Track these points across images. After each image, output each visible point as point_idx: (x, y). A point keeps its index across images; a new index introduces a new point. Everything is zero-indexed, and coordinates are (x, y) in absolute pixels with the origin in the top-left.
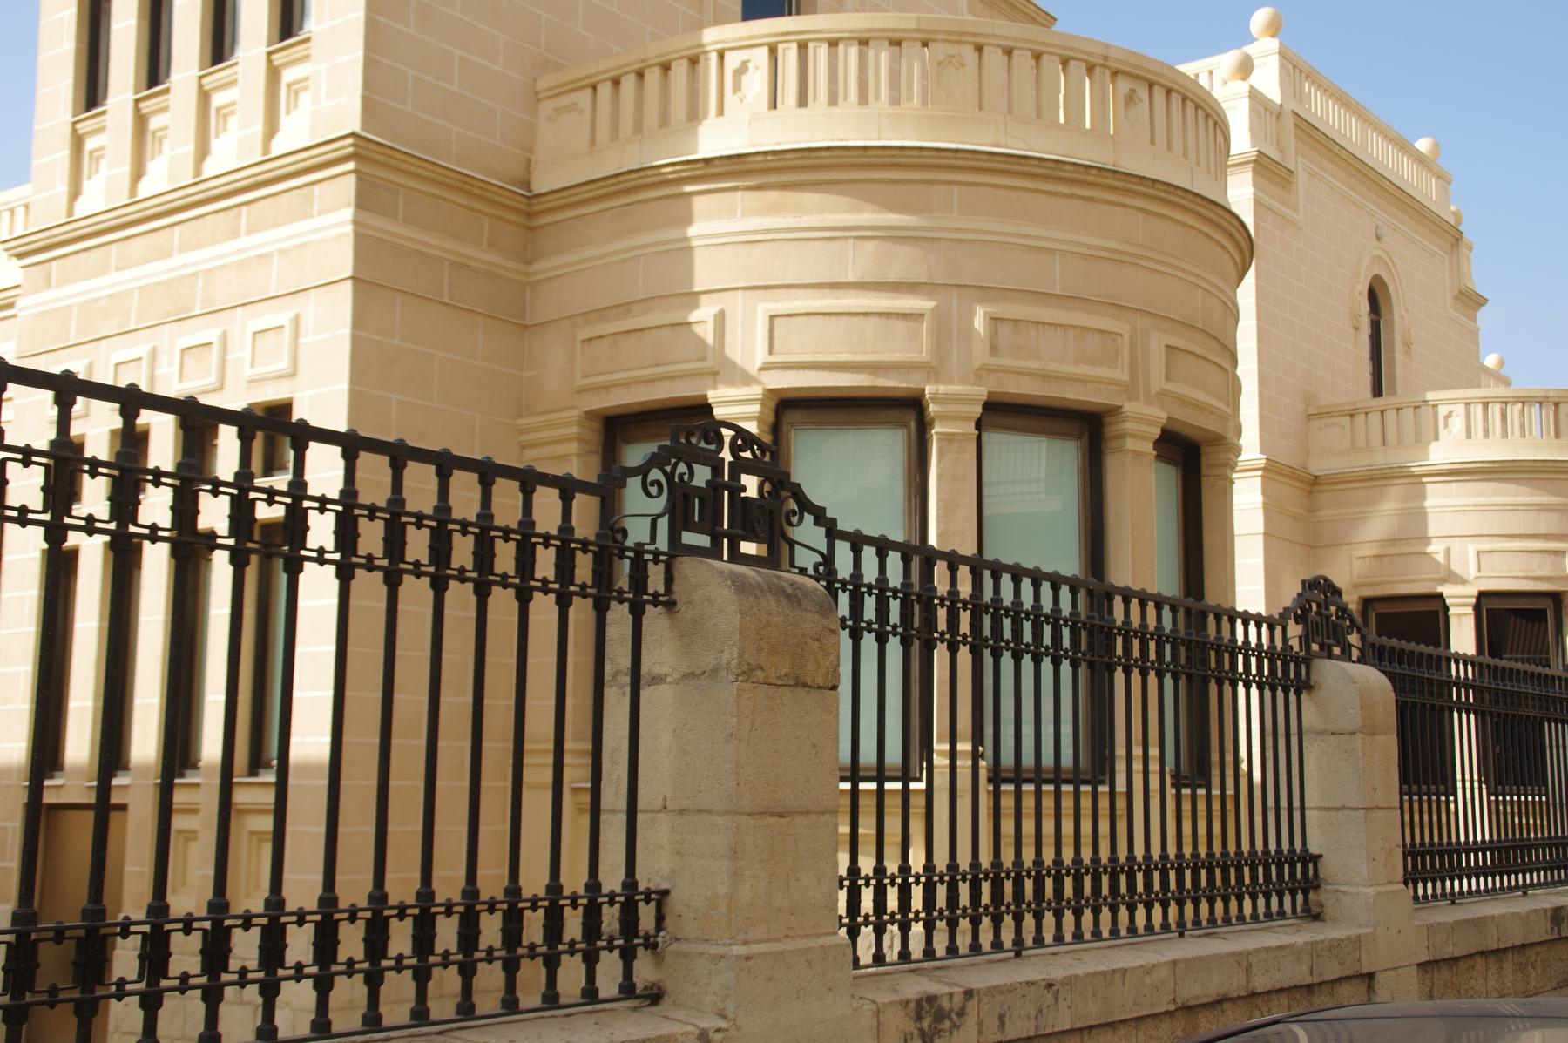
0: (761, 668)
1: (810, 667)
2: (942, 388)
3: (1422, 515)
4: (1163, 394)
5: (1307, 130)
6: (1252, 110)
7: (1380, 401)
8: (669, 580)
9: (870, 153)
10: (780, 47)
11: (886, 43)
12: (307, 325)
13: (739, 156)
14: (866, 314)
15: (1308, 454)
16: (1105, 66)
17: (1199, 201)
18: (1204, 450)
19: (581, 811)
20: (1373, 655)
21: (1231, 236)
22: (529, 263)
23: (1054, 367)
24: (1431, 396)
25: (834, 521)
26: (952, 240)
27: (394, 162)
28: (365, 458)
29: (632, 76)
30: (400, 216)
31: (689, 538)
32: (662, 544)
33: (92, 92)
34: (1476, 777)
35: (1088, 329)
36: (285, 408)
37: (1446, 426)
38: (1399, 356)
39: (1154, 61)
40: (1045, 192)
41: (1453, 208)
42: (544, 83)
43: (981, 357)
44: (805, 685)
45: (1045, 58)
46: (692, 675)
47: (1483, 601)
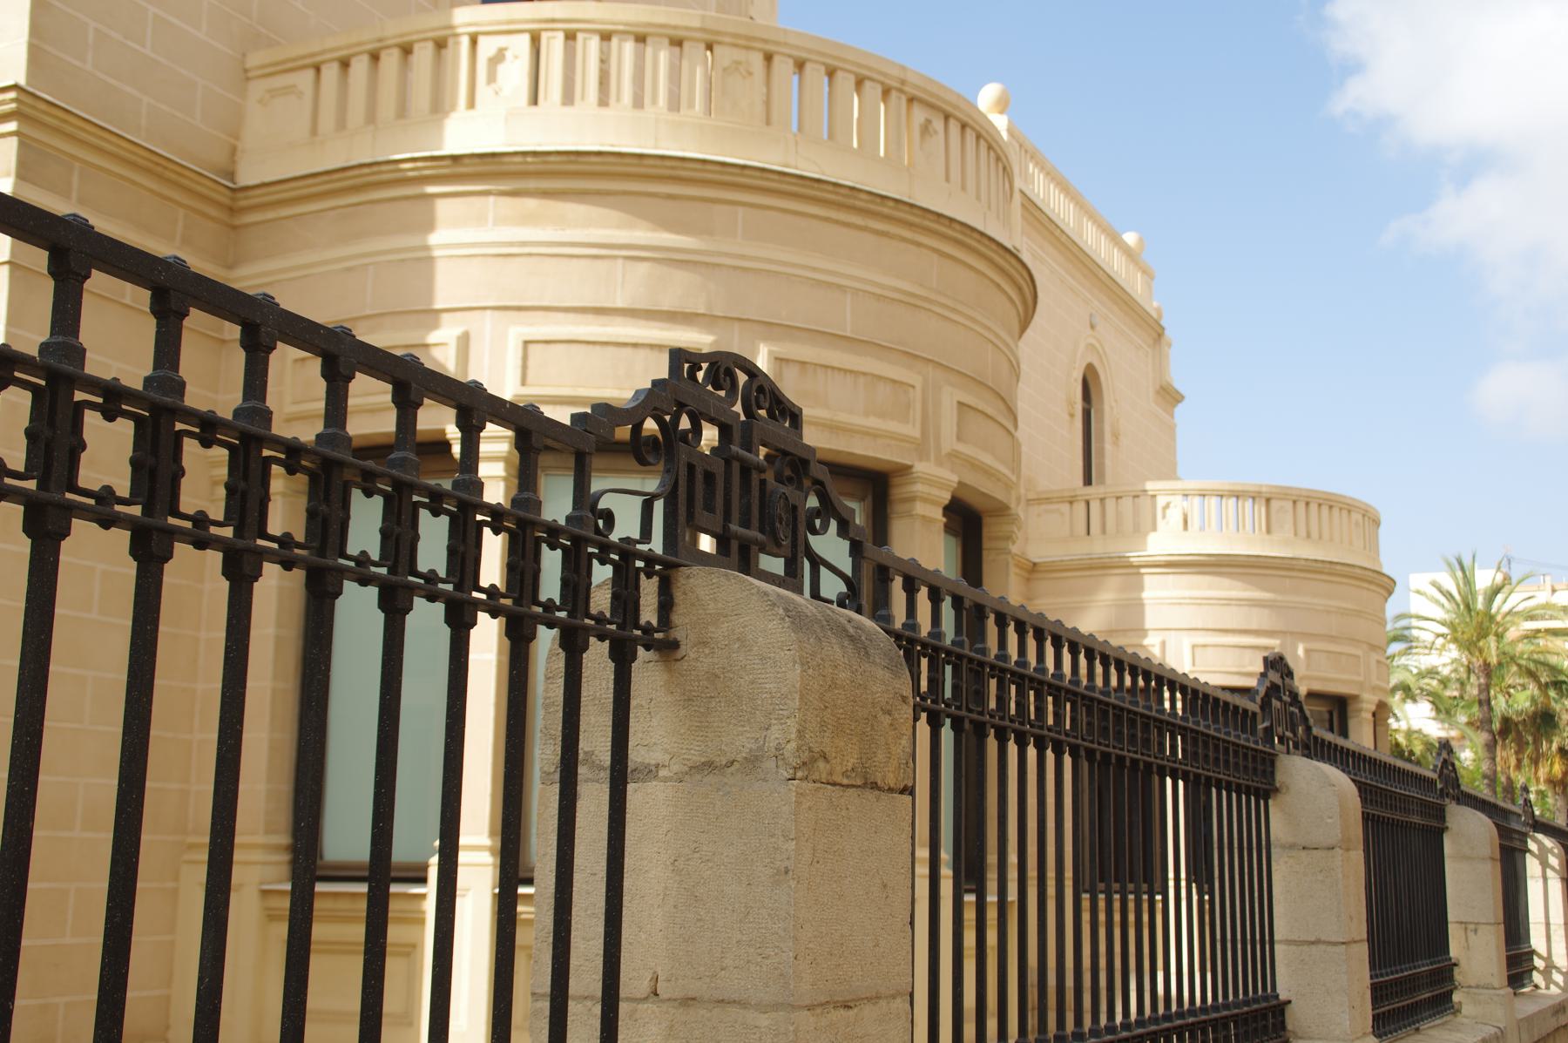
0: (825, 757)
1: (881, 756)
3: (1139, 606)
4: (954, 455)
7: (1089, 490)
8: (666, 606)
9: (646, 162)
10: (544, 36)
11: (666, 41)
13: (494, 155)
14: (635, 345)
16: (901, 91)
17: (994, 246)
18: (987, 521)
19: (272, 917)
21: (1020, 289)
22: (230, 267)
23: (843, 417)
24: (1150, 486)
26: (735, 268)
27: (69, 129)
29: (365, 58)
30: (74, 195)
32: (657, 545)
34: (1183, 875)
35: (880, 378)
37: (1164, 517)
38: (1108, 447)
39: (951, 91)
40: (837, 222)
41: (1155, 304)
42: (255, 60)
44: (874, 786)
45: (840, 74)
46: (709, 766)
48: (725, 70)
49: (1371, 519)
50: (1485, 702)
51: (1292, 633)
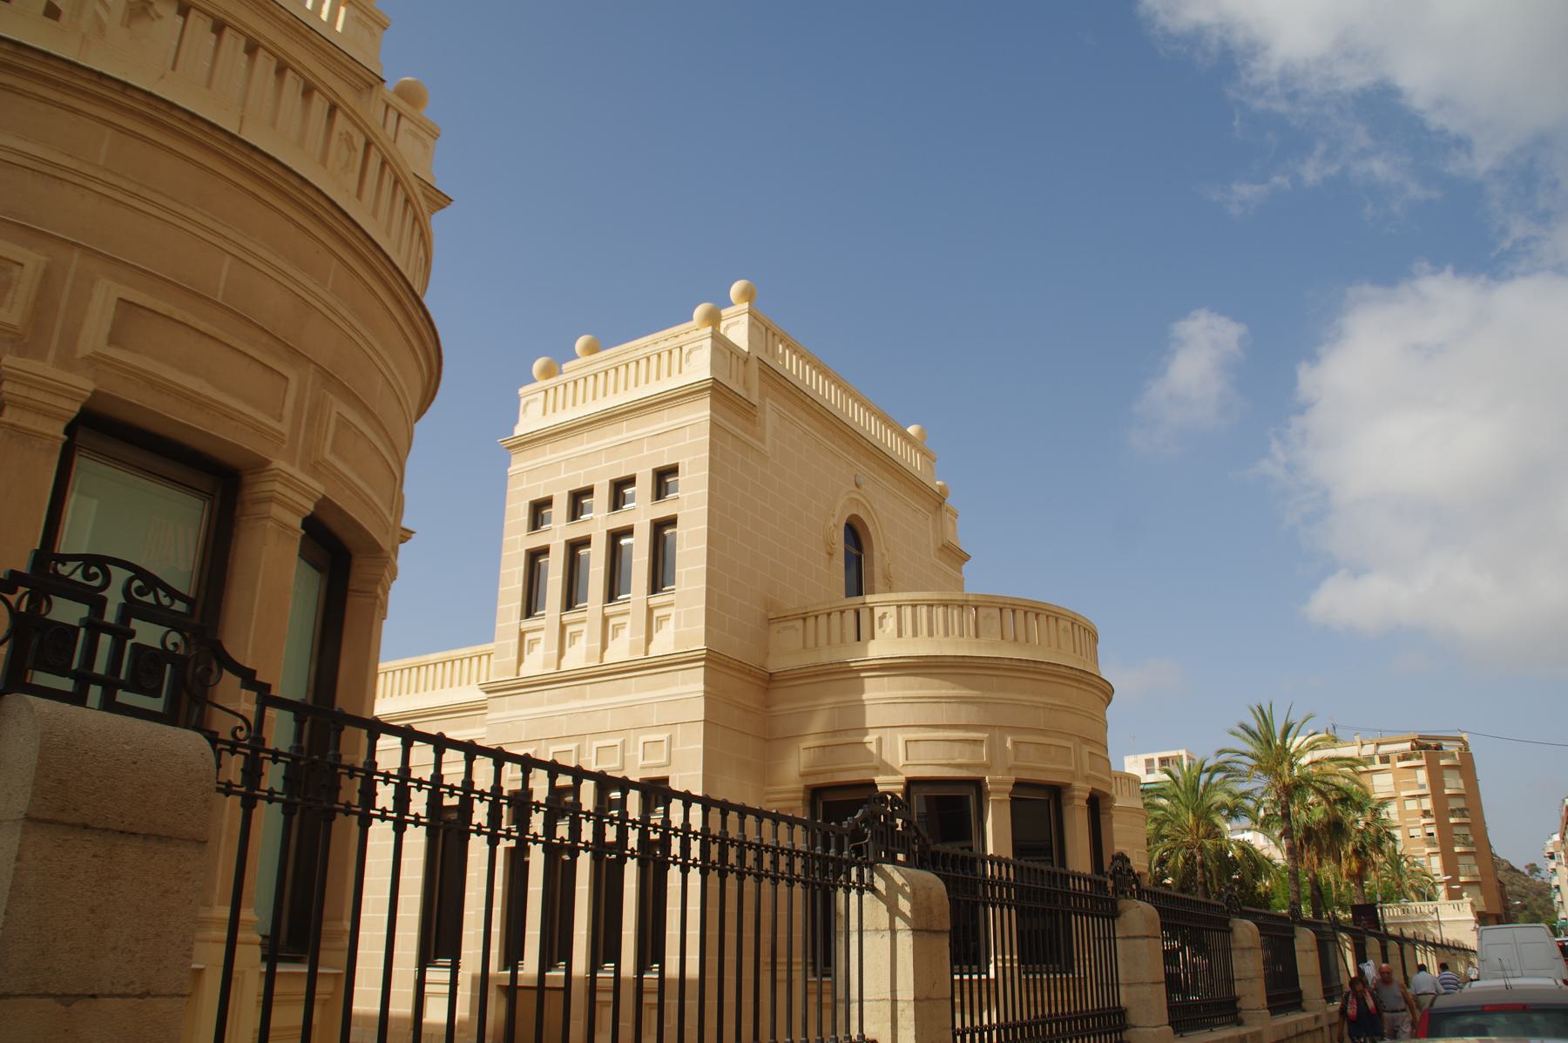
5: (773, 378)
6: (714, 349)
12: (678, 740)
20: (920, 861)
25: (268, 687)
28: (508, 765)
33: (531, 606)
36: (666, 780)
37: (881, 626)
47: (913, 789)
49: (1087, 634)
50: (1286, 816)
51: (1000, 727)
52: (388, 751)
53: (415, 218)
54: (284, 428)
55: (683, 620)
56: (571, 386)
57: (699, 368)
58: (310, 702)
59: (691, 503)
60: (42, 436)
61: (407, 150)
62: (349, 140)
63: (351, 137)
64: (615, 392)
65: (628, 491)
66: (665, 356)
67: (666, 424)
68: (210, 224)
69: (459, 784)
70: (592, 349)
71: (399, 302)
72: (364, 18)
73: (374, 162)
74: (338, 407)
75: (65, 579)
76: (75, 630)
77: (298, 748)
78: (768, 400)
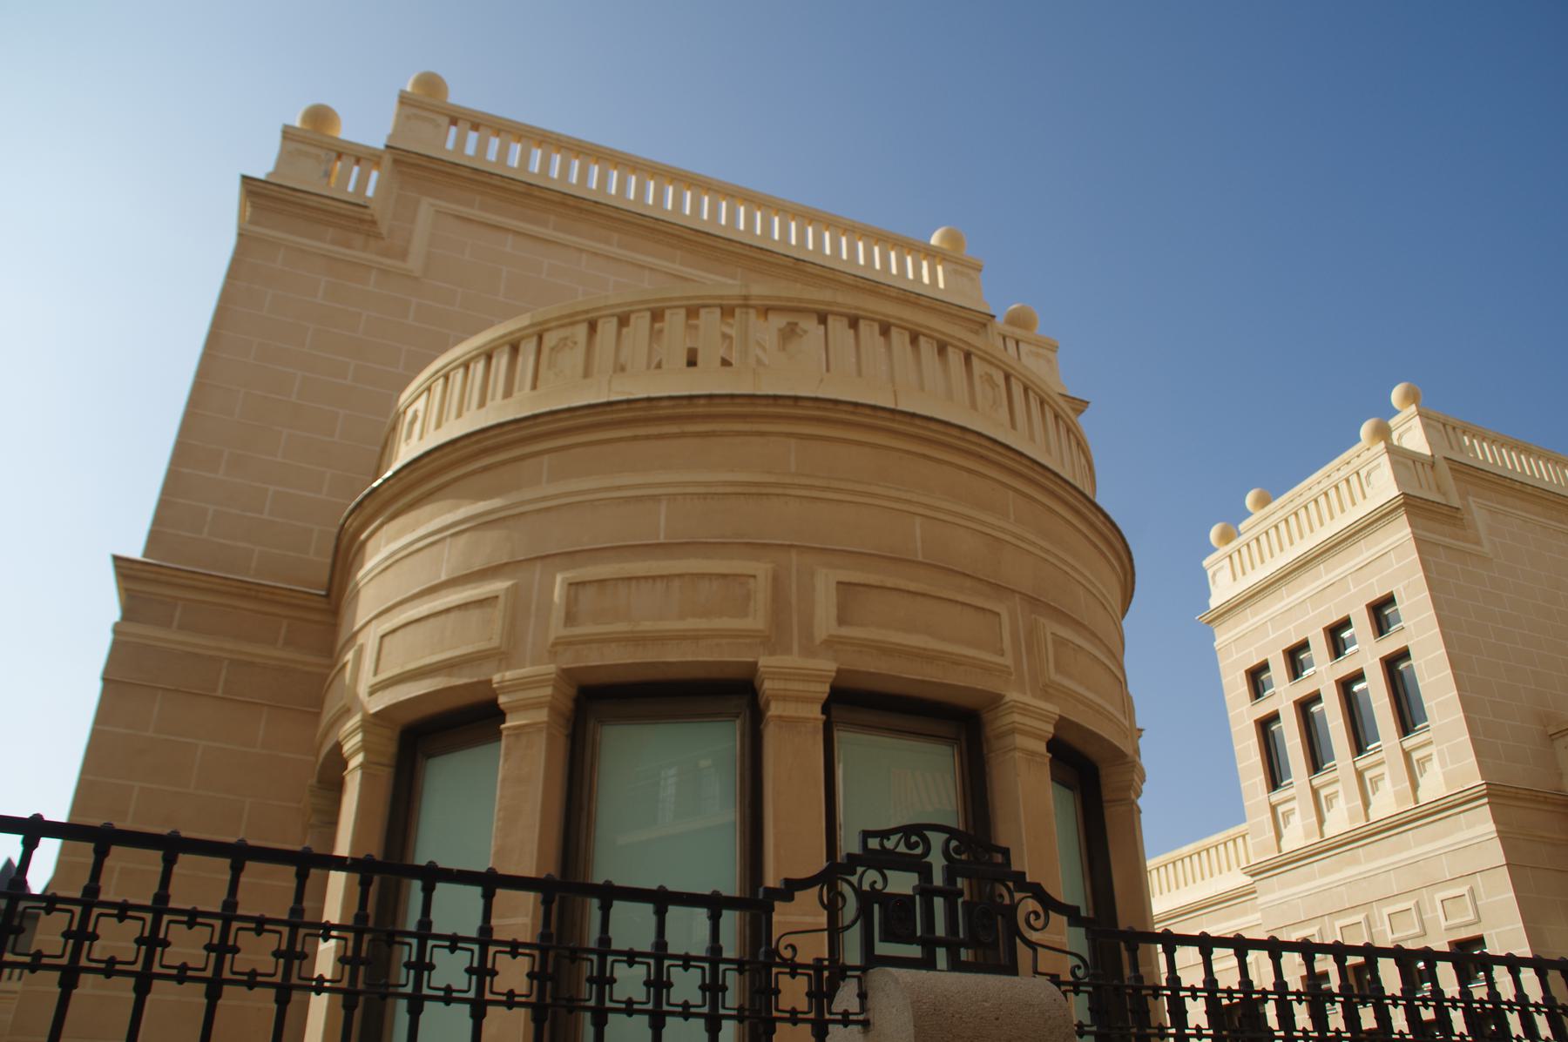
2: (509, 675)
5: (1466, 472)
6: (1394, 464)
15: (1561, 775)
16: (747, 306)
23: (647, 626)
26: (539, 511)
28: (1217, 952)
31: (882, 949)
33: (1275, 776)
36: (1479, 941)
40: (647, 437)
43: (557, 629)
48: (552, 349)
52: (1188, 962)
53: (1068, 430)
54: (1008, 660)
55: (1448, 756)
56: (1254, 545)
57: (1384, 487)
58: (557, 877)
59: (1420, 630)
60: (805, 720)
61: (1031, 364)
62: (989, 379)
63: (991, 377)
64: (1302, 537)
65: (1345, 635)
66: (1343, 486)
67: (1366, 555)
68: (894, 493)
69: (1200, 985)
70: (1263, 502)
71: (1077, 512)
72: (959, 268)
73: (1017, 391)
74: (1051, 628)
75: (892, 852)
76: (911, 898)
77: (545, 936)
78: (1471, 499)
